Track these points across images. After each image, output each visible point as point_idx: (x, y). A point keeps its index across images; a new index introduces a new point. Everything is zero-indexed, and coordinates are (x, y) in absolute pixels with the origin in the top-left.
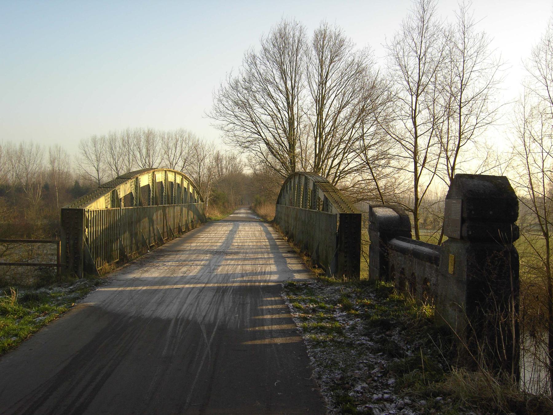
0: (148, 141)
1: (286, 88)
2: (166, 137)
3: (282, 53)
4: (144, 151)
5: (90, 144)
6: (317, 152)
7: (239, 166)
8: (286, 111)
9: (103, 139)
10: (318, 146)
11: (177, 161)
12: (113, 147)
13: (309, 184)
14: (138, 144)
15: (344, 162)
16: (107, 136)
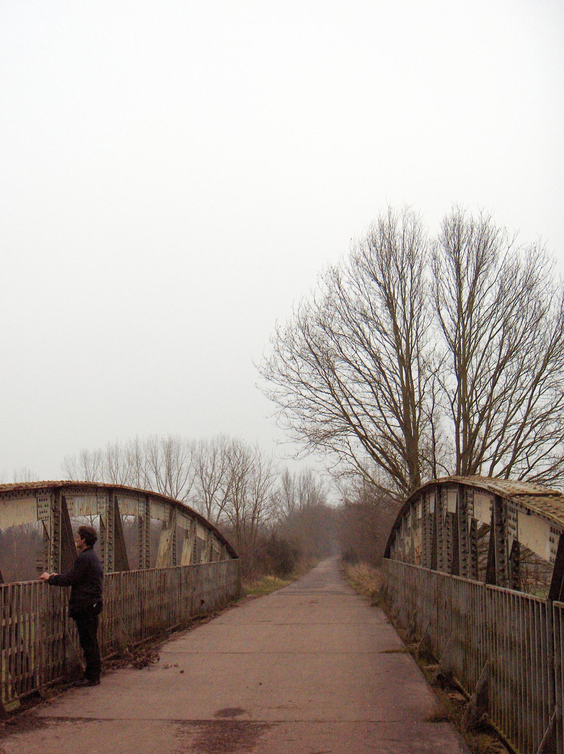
0: (168, 455)
1: (395, 325)
2: (197, 447)
3: (385, 268)
4: (163, 471)
5: (78, 462)
6: (461, 451)
7: (319, 492)
8: (396, 374)
9: (98, 457)
10: (461, 438)
11: (215, 487)
12: (114, 467)
13: (472, 509)
14: (154, 459)
15: (519, 466)
16: (105, 450)
